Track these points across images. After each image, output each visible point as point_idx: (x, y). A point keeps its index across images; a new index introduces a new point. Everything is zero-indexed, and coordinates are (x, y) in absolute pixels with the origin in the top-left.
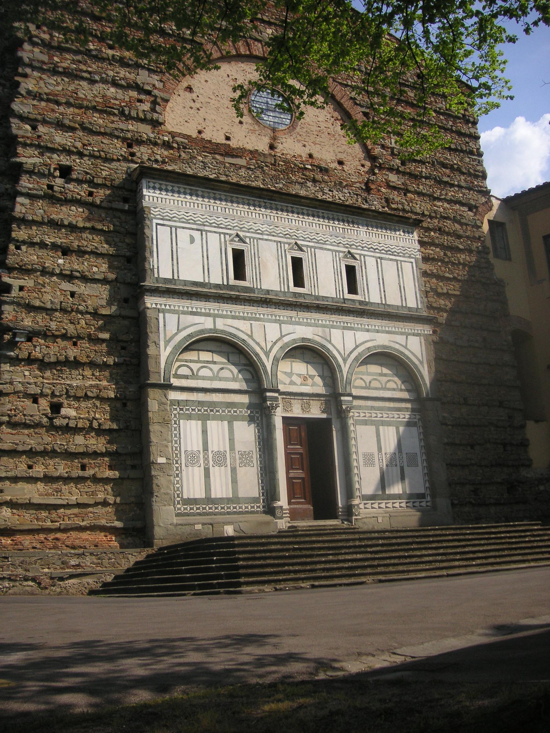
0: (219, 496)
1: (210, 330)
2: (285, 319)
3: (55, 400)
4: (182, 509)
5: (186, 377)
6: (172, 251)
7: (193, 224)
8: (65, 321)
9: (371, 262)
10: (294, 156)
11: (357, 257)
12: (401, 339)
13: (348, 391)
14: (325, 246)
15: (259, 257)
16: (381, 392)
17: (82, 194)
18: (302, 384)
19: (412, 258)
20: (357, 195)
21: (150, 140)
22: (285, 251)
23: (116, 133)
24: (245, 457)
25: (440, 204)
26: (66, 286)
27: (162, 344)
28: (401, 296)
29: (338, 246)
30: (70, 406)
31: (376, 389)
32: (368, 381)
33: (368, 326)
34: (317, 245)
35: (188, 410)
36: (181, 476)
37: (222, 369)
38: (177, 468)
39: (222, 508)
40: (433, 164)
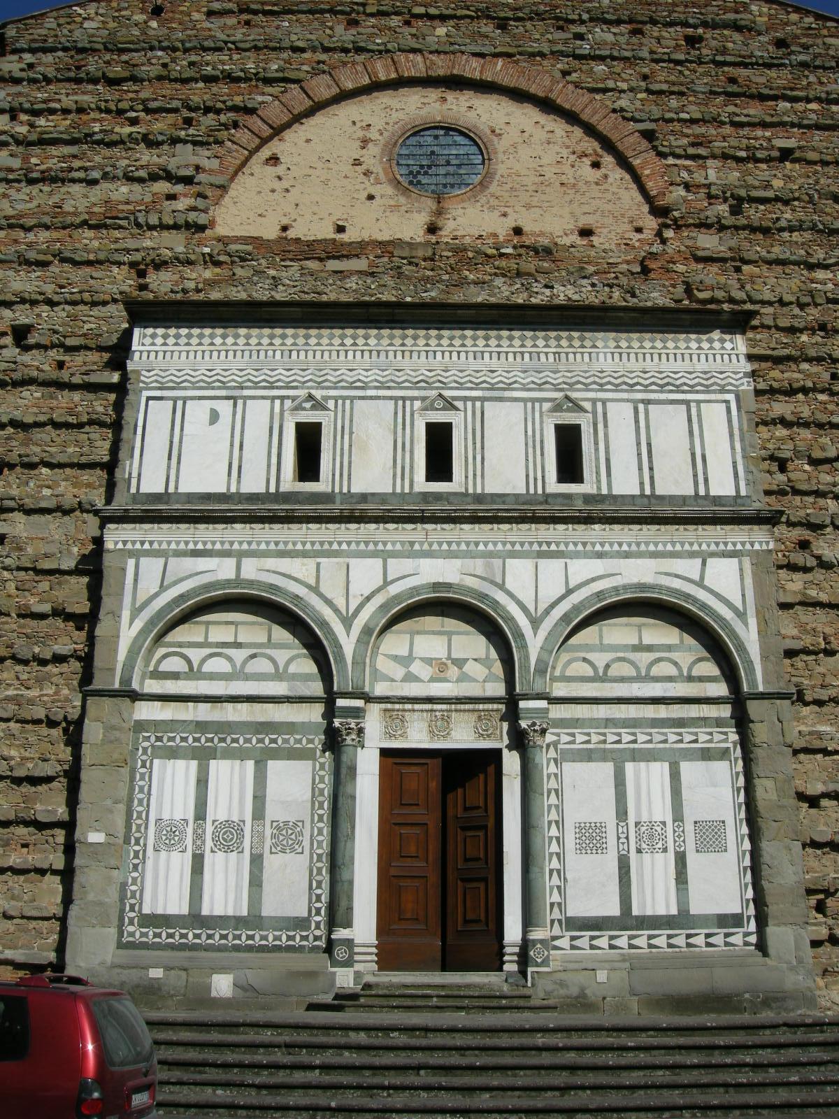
0: (219, 911)
1: (228, 583)
2: (398, 547)
5: (175, 676)
6: (171, 442)
7: (219, 388)
9: (620, 414)
12: (690, 567)
13: (538, 687)
14: (507, 394)
15: (351, 433)
16: (635, 685)
17: (46, 367)
18: (432, 680)
19: (729, 392)
20: (611, 286)
21: (177, 258)
22: (412, 415)
23: (117, 257)
24: (287, 836)
27: (126, 615)
28: (695, 476)
31: (622, 680)
33: (602, 545)
34: (488, 394)
36: (143, 870)
38: (136, 853)
39: (224, 937)
40: (811, 201)
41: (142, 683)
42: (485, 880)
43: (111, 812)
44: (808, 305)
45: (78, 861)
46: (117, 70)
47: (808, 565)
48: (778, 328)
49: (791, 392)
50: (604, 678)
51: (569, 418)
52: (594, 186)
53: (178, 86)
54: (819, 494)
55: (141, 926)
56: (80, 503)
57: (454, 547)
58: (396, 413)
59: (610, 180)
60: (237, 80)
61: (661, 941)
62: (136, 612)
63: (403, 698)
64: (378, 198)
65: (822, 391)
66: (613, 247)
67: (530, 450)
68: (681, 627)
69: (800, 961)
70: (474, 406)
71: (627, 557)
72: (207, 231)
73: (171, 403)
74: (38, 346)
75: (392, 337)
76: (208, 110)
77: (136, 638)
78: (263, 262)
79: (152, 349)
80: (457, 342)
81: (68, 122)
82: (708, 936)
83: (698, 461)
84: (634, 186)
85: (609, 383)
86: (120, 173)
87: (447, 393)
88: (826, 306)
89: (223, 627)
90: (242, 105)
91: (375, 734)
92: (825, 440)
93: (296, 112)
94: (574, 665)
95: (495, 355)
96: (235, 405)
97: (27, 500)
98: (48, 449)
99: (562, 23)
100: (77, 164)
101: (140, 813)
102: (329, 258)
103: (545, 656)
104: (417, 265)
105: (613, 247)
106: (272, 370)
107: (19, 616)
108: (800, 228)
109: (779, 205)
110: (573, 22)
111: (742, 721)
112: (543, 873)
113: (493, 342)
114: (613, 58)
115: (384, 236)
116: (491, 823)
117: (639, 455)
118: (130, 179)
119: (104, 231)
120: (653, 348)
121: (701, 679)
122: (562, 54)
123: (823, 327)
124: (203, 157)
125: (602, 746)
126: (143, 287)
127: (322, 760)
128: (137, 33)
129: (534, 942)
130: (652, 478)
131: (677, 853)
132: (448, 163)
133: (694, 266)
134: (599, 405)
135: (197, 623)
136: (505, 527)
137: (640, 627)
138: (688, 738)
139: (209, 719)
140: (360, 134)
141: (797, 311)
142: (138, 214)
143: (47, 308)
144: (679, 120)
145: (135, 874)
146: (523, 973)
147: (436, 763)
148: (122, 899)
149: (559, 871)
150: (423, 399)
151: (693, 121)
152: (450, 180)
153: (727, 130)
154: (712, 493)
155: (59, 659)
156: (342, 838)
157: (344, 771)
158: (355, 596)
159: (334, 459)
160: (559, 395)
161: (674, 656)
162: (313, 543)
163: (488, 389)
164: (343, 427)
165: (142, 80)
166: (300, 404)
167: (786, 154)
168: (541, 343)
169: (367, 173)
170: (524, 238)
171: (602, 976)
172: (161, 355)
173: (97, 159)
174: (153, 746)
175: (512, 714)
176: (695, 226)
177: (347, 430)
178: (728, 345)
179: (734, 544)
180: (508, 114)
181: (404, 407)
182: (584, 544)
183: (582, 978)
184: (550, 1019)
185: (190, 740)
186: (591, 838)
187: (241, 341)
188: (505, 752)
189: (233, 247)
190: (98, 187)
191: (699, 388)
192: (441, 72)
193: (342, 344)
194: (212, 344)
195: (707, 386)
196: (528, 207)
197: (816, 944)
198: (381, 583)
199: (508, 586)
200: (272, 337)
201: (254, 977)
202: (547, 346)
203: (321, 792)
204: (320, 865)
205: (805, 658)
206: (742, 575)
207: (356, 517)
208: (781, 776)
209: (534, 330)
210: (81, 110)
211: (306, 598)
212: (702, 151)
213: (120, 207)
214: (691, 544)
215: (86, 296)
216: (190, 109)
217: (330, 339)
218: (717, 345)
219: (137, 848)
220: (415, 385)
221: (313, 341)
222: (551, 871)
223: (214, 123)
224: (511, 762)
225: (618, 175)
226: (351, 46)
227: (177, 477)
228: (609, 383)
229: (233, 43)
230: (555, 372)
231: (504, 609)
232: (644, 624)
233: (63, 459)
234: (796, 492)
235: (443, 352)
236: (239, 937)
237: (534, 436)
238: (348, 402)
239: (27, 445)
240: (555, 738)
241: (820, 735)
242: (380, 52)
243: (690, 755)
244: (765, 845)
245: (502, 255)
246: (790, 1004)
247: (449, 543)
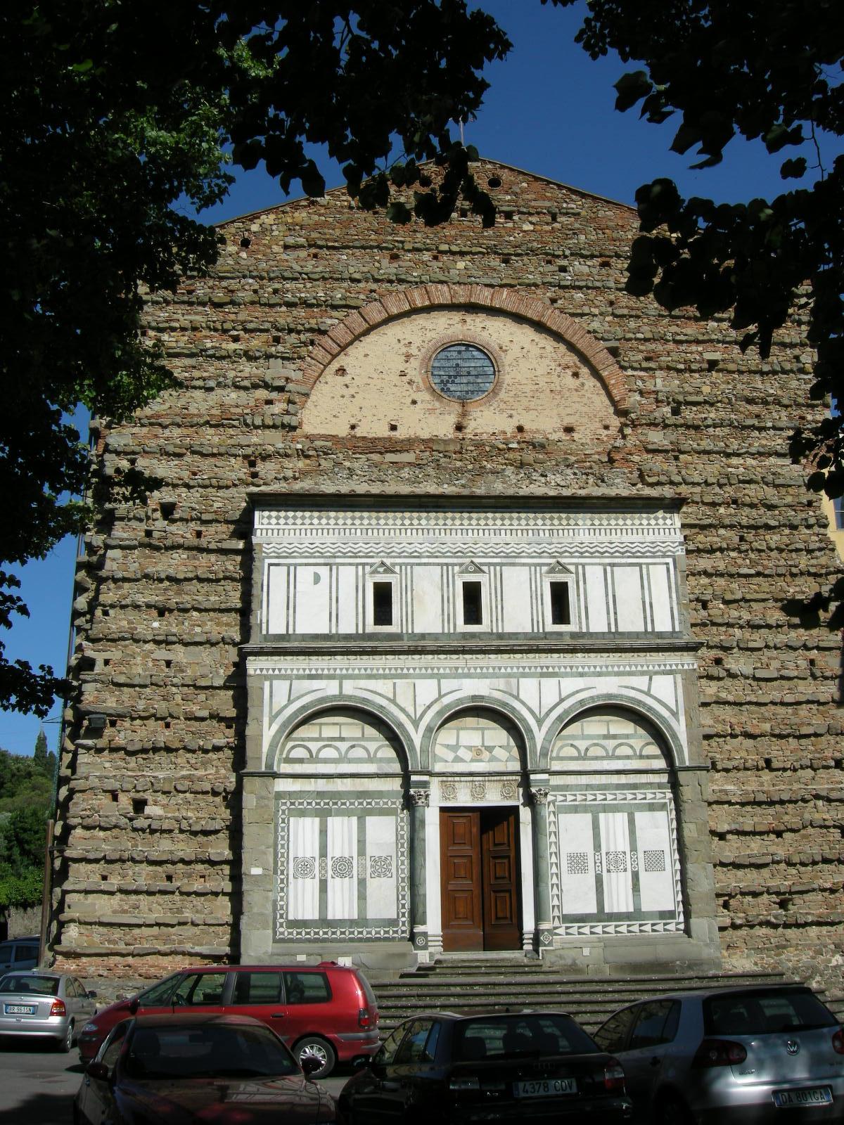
0: (339, 916)
3: (138, 796)
4: (286, 933)
5: (301, 761)
6: (288, 597)
7: (319, 557)
8: (157, 698)
9: (594, 574)
11: (572, 568)
12: (641, 682)
13: (542, 766)
14: (517, 560)
15: (412, 590)
16: (605, 762)
17: (188, 535)
18: (472, 761)
19: (668, 556)
20: (587, 474)
21: (278, 453)
22: (453, 577)
23: (233, 451)
24: (381, 867)
25: (740, 461)
26: (162, 654)
27: (266, 720)
28: (645, 618)
29: (541, 557)
30: (156, 803)
31: (596, 758)
32: (582, 749)
34: (504, 560)
37: (353, 747)
39: (343, 933)
40: (730, 403)
42: (509, 891)
43: (265, 853)
45: (245, 887)
46: (220, 296)
49: (711, 551)
51: (560, 578)
52: (574, 393)
53: (267, 309)
54: (729, 625)
55: (288, 928)
56: (223, 638)
57: (485, 670)
59: (586, 387)
60: (311, 306)
61: (623, 929)
64: (419, 403)
65: (733, 550)
66: (588, 441)
67: (534, 601)
69: (711, 940)
70: (495, 570)
72: (298, 430)
74: (181, 519)
76: (290, 331)
77: (274, 736)
78: (341, 455)
80: (482, 522)
81: (186, 338)
82: (653, 925)
83: (647, 608)
84: (603, 392)
86: (229, 382)
87: (476, 560)
90: (316, 327)
92: (735, 586)
93: (356, 333)
94: (565, 749)
96: (331, 570)
97: (185, 636)
98: (195, 597)
99: (550, 258)
100: (196, 374)
101: (283, 854)
102: (387, 452)
103: (546, 744)
105: (588, 441)
107: (186, 719)
108: (721, 426)
109: (707, 407)
110: (558, 256)
111: (675, 785)
112: (547, 887)
113: (507, 522)
114: (588, 288)
115: (425, 435)
116: (512, 854)
117: (607, 603)
118: (237, 387)
119: (222, 429)
120: (617, 525)
121: (648, 757)
122: (550, 284)
123: (735, 502)
124: (290, 370)
126: (254, 475)
128: (232, 263)
129: (543, 931)
130: (616, 620)
131: (633, 872)
132: (469, 374)
133: (646, 456)
134: (580, 567)
136: (519, 656)
138: (640, 796)
140: (404, 350)
141: (717, 490)
142: (246, 417)
143: (185, 490)
144: (636, 339)
145: (282, 894)
146: (536, 951)
148: (275, 910)
149: (557, 885)
150: (461, 565)
151: (646, 340)
152: (470, 388)
153: (671, 346)
154: (657, 630)
155: (217, 749)
156: (417, 865)
157: (417, 823)
160: (553, 561)
161: (631, 741)
162: (390, 669)
163: (505, 557)
165: (239, 304)
166: (376, 570)
167: (713, 365)
168: (540, 522)
169: (410, 383)
170: (525, 435)
171: (586, 952)
173: (211, 369)
175: (525, 782)
176: (647, 425)
177: (409, 588)
178: (669, 522)
179: (671, 665)
180: (511, 334)
182: (571, 667)
183: (573, 953)
184: (552, 978)
185: (314, 804)
186: (578, 863)
187: (332, 521)
188: (521, 808)
189: (318, 443)
190: (214, 393)
191: (648, 554)
192: (462, 300)
194: (311, 524)
196: (527, 409)
197: (722, 929)
199: (521, 697)
200: (353, 518)
201: (365, 958)
204: (403, 884)
205: (718, 739)
206: (675, 687)
210: (194, 329)
212: (652, 365)
213: (233, 410)
214: (642, 666)
215: (214, 481)
216: (278, 330)
218: (661, 522)
219: (282, 877)
220: (455, 555)
221: (382, 522)
222: (553, 885)
223: (296, 341)
224: (525, 814)
225: (591, 383)
226: (394, 278)
227: (294, 622)
229: (306, 274)
230: (550, 544)
231: (519, 713)
233: (208, 605)
234: (714, 624)
235: (473, 530)
236: (353, 933)
238: (409, 567)
239: (180, 594)
240: (553, 798)
241: (726, 792)
242: (416, 283)
243: (641, 808)
244: (689, 866)
245: (510, 449)
246: (705, 967)
247: (482, 668)
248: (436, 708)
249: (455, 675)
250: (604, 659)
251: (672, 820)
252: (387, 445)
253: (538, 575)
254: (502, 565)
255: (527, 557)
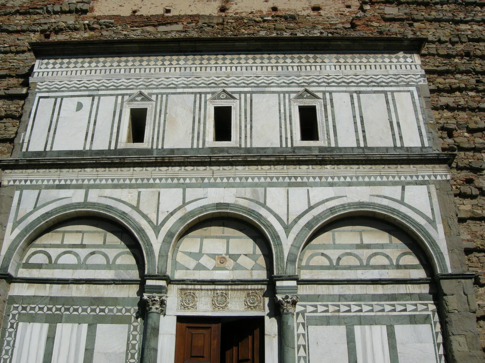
1: (79, 205)
5: (39, 266)
6: (51, 122)
7: (84, 90)
9: (341, 100)
10: (252, 13)
11: (320, 95)
12: (395, 192)
13: (290, 271)
15: (166, 113)
18: (215, 268)
19: (411, 86)
21: (69, 27)
22: (206, 102)
23: (34, 28)
27: (10, 225)
28: (393, 135)
31: (350, 268)
32: (334, 258)
33: (333, 178)
35: (33, 309)
41: (17, 271)
44: (457, 42)
47: (474, 193)
48: (439, 55)
49: (451, 90)
50: (337, 267)
51: (308, 102)
57: (231, 180)
58: (195, 102)
62: (16, 224)
63: (194, 281)
65: (471, 90)
66: (333, 15)
67: (283, 121)
68: (390, 232)
70: (245, 97)
71: (350, 186)
72: (88, 14)
73: (53, 100)
75: (194, 60)
78: (120, 28)
79: (45, 71)
80: (235, 61)
83: (394, 126)
85: (334, 82)
87: (228, 90)
88: (468, 43)
89: (74, 234)
91: (174, 304)
94: (316, 258)
95: (259, 68)
96: (93, 100)
102: (159, 25)
103: (294, 251)
104: (213, 27)
106: (118, 80)
111: (437, 295)
119: (28, 16)
121: (406, 267)
123: (468, 54)
125: (337, 314)
127: (135, 324)
133: (383, 23)
134: (328, 95)
135: (57, 232)
136: (267, 167)
137: (361, 232)
138: (399, 308)
139: (59, 295)
141: (450, 46)
142: (48, 6)
147: (216, 328)
150: (213, 93)
154: (406, 145)
158: (163, 212)
159: (154, 129)
160: (302, 89)
161: (387, 251)
162: (137, 180)
163: (255, 87)
164: (161, 111)
172: (50, 74)
174: (19, 313)
177: (163, 112)
179: (423, 176)
181: (200, 98)
182: (320, 178)
188: (267, 319)
191: (392, 84)
193: (163, 64)
195: (397, 83)
198: (181, 204)
199: (268, 204)
200: (119, 62)
202: (292, 62)
203: (134, 346)
206: (430, 196)
207: (165, 163)
208: (469, 334)
209: (284, 54)
211: (130, 214)
214: (394, 177)
215: (13, 48)
217: (156, 62)
218: (402, 60)
220: (208, 86)
221: (145, 63)
224: (271, 326)
228: (334, 82)
230: (298, 77)
231: (265, 219)
232: (364, 231)
237: (285, 113)
240: (303, 308)
243: (401, 320)
245: (265, 21)
247: (228, 178)
248: (179, 214)
249: (202, 184)
250: (354, 170)
251: (437, 333)
252: (160, 20)
253: (287, 101)
254: (251, 93)
255: (277, 87)
